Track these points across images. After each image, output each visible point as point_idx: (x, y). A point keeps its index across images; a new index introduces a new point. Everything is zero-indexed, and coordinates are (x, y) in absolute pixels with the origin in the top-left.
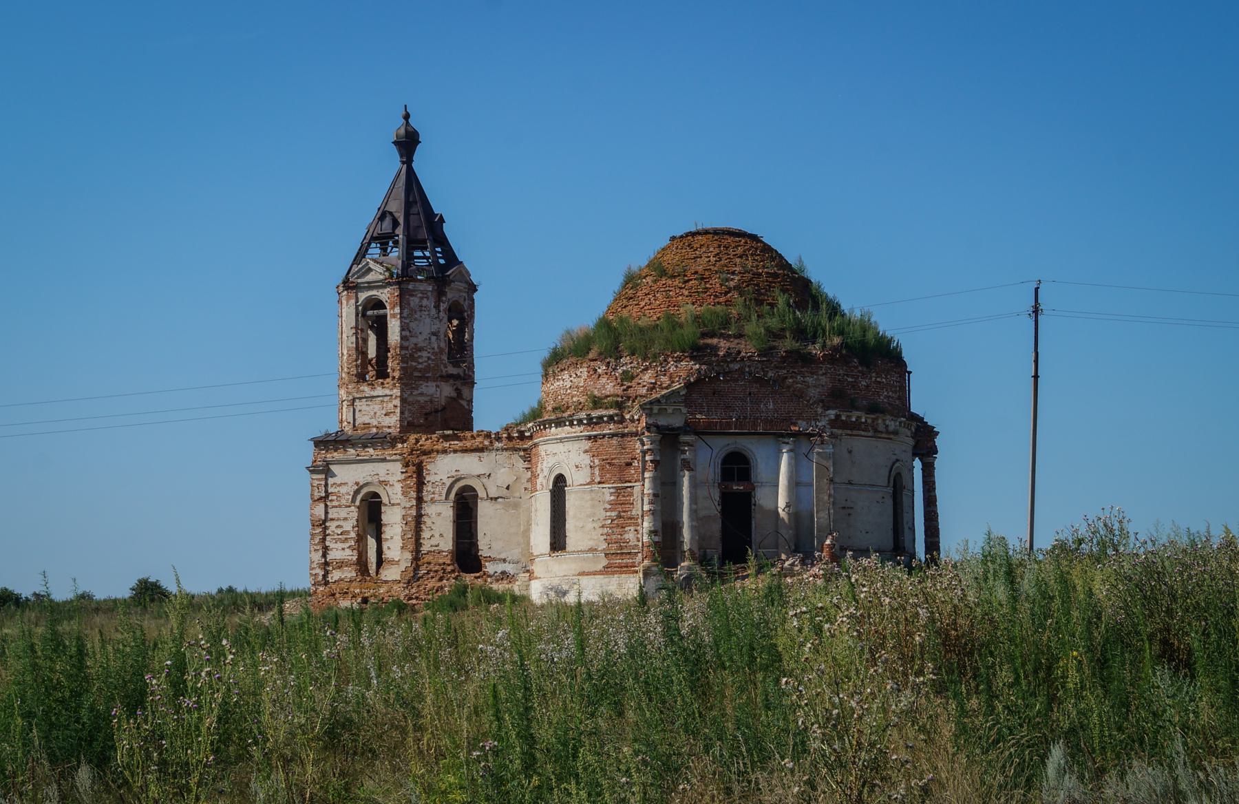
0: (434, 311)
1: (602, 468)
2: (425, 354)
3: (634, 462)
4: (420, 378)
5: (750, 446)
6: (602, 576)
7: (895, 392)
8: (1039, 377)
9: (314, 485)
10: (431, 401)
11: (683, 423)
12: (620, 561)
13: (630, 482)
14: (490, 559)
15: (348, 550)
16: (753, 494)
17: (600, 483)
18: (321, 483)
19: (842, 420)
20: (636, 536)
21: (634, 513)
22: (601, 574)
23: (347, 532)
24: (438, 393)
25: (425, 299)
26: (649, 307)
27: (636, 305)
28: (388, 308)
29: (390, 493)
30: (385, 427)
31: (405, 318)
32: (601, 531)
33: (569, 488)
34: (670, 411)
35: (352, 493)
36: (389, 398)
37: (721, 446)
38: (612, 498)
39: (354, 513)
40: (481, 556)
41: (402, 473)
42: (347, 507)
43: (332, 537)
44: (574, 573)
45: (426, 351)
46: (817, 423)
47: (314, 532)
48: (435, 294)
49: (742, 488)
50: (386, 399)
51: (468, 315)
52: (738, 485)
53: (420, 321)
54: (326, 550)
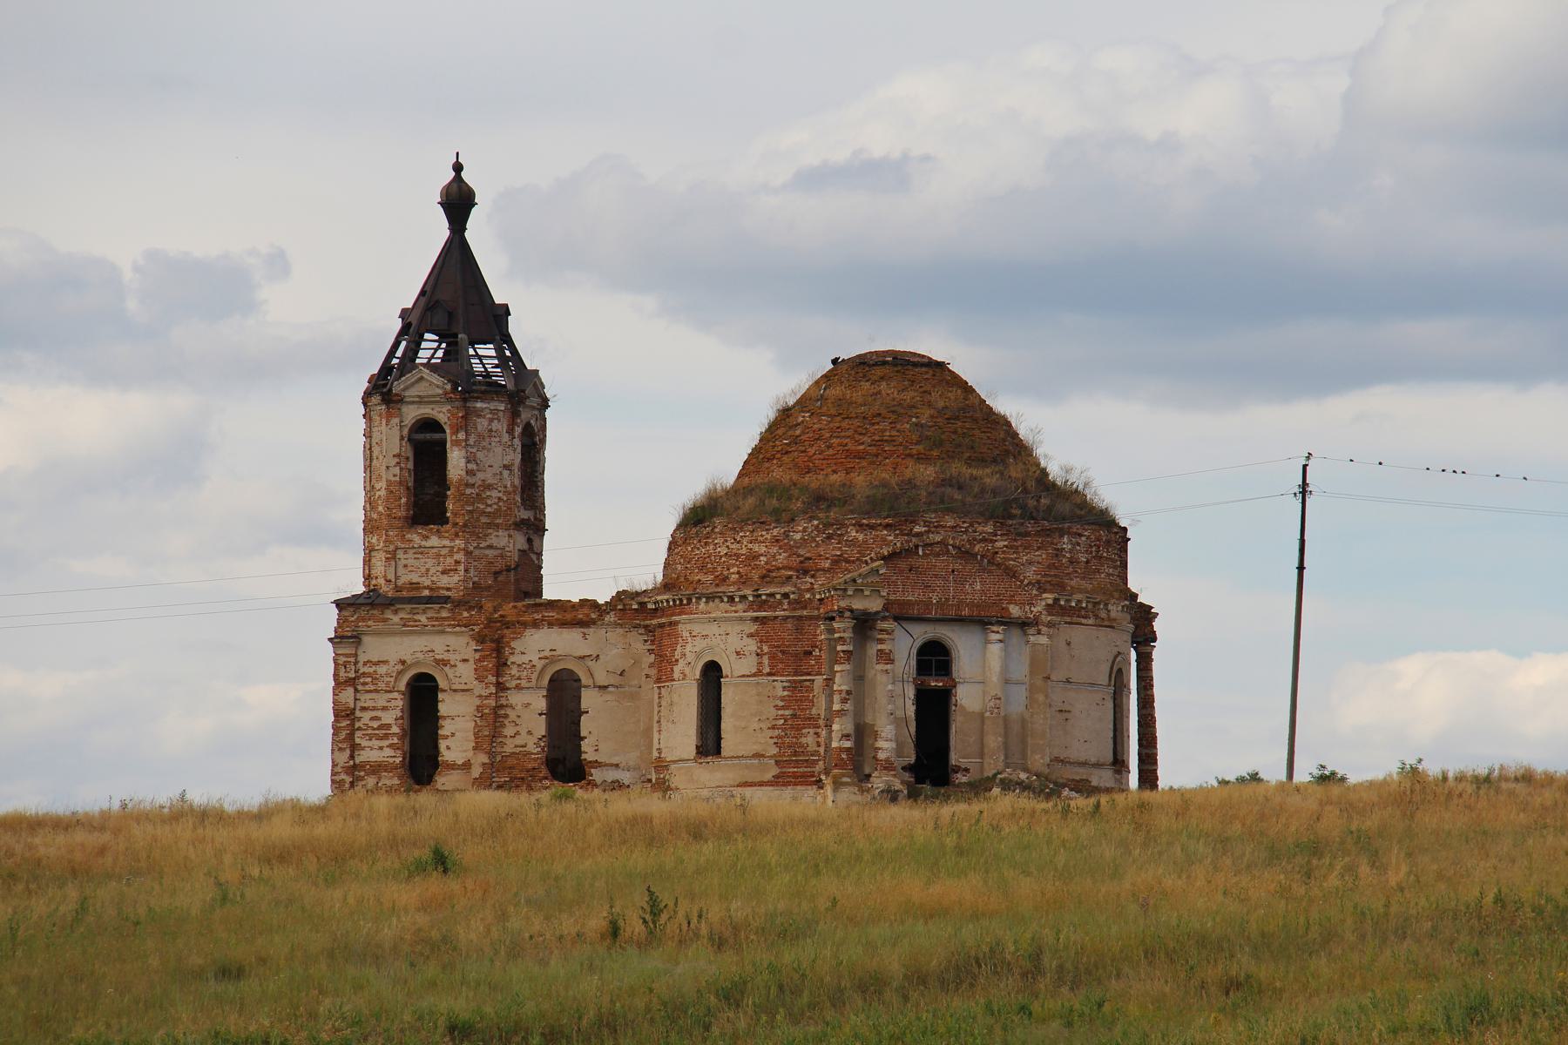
0: (506, 437)
1: (772, 657)
2: (495, 494)
3: (814, 651)
4: (489, 525)
5: (950, 634)
6: (771, 788)
7: (1115, 567)
8: (1304, 568)
9: (339, 662)
10: (502, 556)
11: (881, 607)
12: (795, 770)
13: (809, 674)
14: (957, 769)
15: (388, 749)
16: (953, 691)
17: (769, 674)
18: (349, 659)
19: (1060, 605)
20: (817, 740)
21: (814, 711)
22: (770, 786)
23: (388, 726)
24: (511, 545)
25: (496, 421)
26: (821, 457)
27: (802, 452)
28: (448, 431)
29: (451, 676)
30: (443, 588)
31: (472, 446)
32: (770, 733)
33: (727, 679)
34: (867, 593)
35: (394, 675)
36: (448, 549)
37: (924, 632)
38: (786, 693)
39: (398, 702)
40: (585, 760)
41: (475, 650)
42: (387, 692)
43: (364, 732)
44: (732, 783)
45: (496, 489)
46: (1032, 609)
47: (338, 725)
48: (508, 414)
49: (941, 684)
50: (444, 552)
51: (540, 440)
52: (936, 681)
53: (489, 450)
54: (354, 748)
